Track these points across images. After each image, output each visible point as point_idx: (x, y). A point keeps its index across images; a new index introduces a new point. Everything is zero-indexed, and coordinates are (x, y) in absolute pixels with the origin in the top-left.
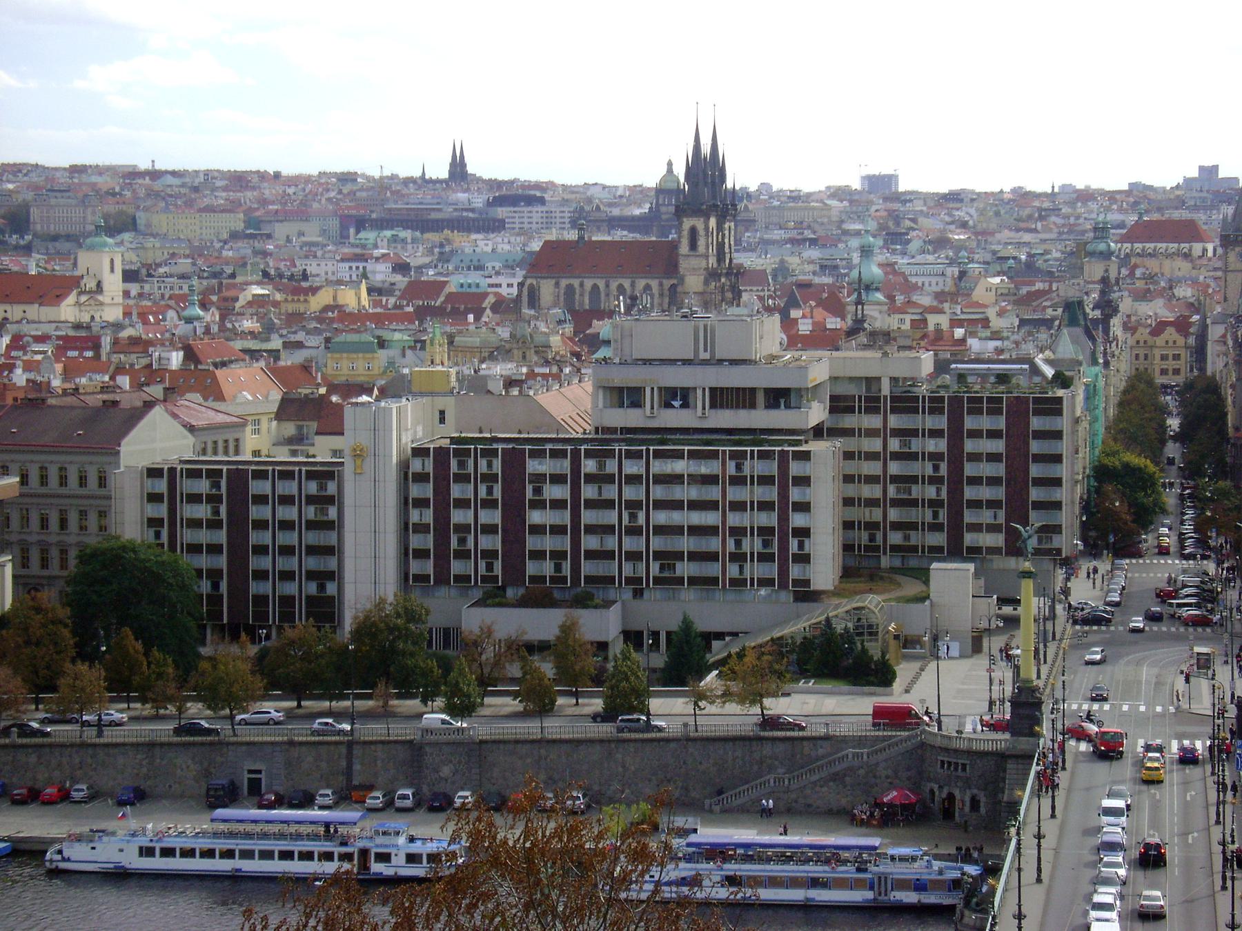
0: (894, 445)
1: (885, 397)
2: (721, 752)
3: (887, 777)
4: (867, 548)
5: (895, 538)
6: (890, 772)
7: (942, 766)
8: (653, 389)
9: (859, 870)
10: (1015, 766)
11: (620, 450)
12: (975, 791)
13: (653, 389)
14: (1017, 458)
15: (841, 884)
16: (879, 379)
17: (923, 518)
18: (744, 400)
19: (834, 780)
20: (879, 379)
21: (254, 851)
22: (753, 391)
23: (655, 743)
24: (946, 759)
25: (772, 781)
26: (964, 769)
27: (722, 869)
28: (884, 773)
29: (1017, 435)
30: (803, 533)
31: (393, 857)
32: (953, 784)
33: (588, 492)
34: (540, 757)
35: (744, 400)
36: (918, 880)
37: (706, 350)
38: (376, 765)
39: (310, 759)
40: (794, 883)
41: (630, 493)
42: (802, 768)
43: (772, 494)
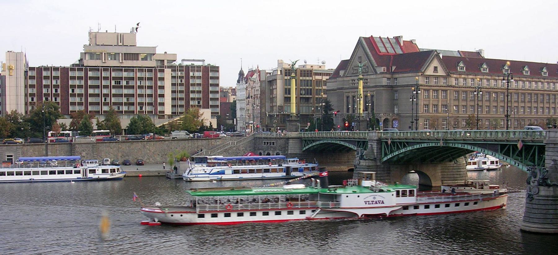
0: (124, 100)
1: (166, 66)
2: (184, 144)
3: (243, 150)
6: (244, 148)
7: (265, 144)
8: (105, 53)
9: (279, 166)
10: (292, 141)
12: (278, 151)
13: (105, 53)
14: (206, 85)
15: (275, 171)
16: (164, 60)
18: (133, 58)
19: (225, 152)
21: (39, 171)
23: (160, 142)
24: (266, 141)
25: (231, 143)
26: (273, 144)
27: (231, 168)
28: (242, 149)
29: (206, 77)
31: (97, 171)
32: (269, 149)
34: (119, 148)
35: (133, 58)
36: (300, 168)
37: (121, 42)
38: (57, 153)
39: (31, 151)
40: (259, 171)
42: (212, 149)
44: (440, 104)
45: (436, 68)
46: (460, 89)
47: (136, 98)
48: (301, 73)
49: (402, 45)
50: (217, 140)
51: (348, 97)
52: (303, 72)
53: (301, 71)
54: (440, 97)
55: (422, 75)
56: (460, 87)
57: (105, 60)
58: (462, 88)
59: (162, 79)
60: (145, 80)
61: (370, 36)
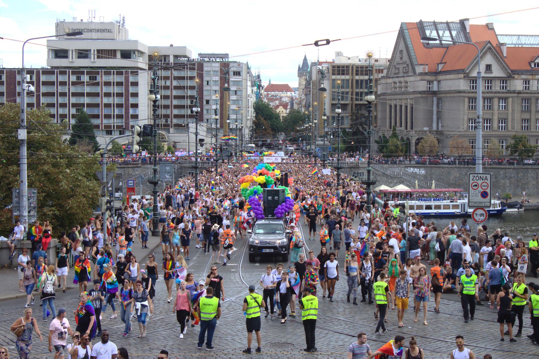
4: (165, 125)
5: (175, 121)
11: (57, 71)
16: (169, 56)
17: (187, 113)
20: (169, 56)
22: (115, 51)
30: (135, 106)
33: (43, 100)
41: (61, 111)
43: (122, 101)
44: (496, 118)
45: (489, 68)
46: (533, 95)
47: (102, 109)
48: (333, 70)
49: (468, 31)
50: (136, 169)
51: (391, 106)
52: (360, 69)
53: (357, 67)
54: (496, 107)
55: (464, 77)
56: (531, 93)
57: (72, 58)
58: (535, 93)
59: (135, 84)
60: (114, 85)
61: (418, 21)
